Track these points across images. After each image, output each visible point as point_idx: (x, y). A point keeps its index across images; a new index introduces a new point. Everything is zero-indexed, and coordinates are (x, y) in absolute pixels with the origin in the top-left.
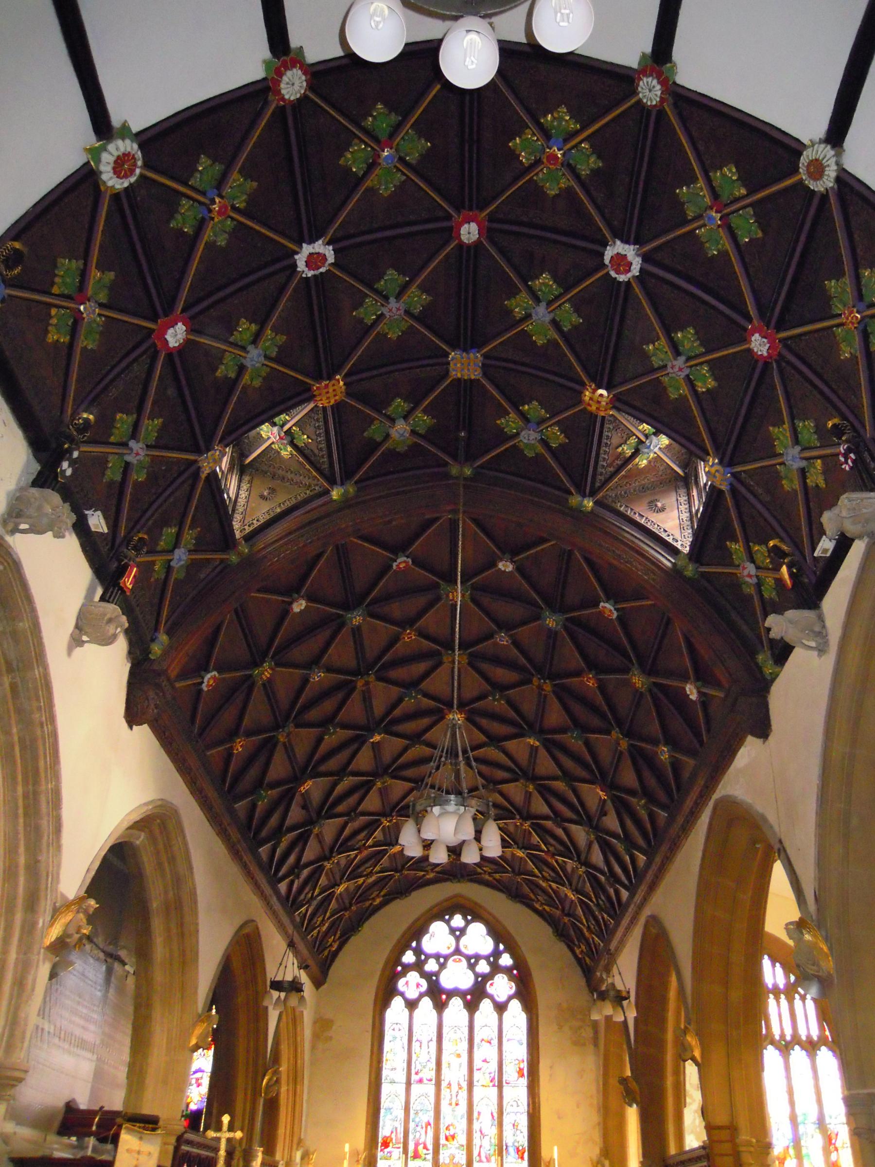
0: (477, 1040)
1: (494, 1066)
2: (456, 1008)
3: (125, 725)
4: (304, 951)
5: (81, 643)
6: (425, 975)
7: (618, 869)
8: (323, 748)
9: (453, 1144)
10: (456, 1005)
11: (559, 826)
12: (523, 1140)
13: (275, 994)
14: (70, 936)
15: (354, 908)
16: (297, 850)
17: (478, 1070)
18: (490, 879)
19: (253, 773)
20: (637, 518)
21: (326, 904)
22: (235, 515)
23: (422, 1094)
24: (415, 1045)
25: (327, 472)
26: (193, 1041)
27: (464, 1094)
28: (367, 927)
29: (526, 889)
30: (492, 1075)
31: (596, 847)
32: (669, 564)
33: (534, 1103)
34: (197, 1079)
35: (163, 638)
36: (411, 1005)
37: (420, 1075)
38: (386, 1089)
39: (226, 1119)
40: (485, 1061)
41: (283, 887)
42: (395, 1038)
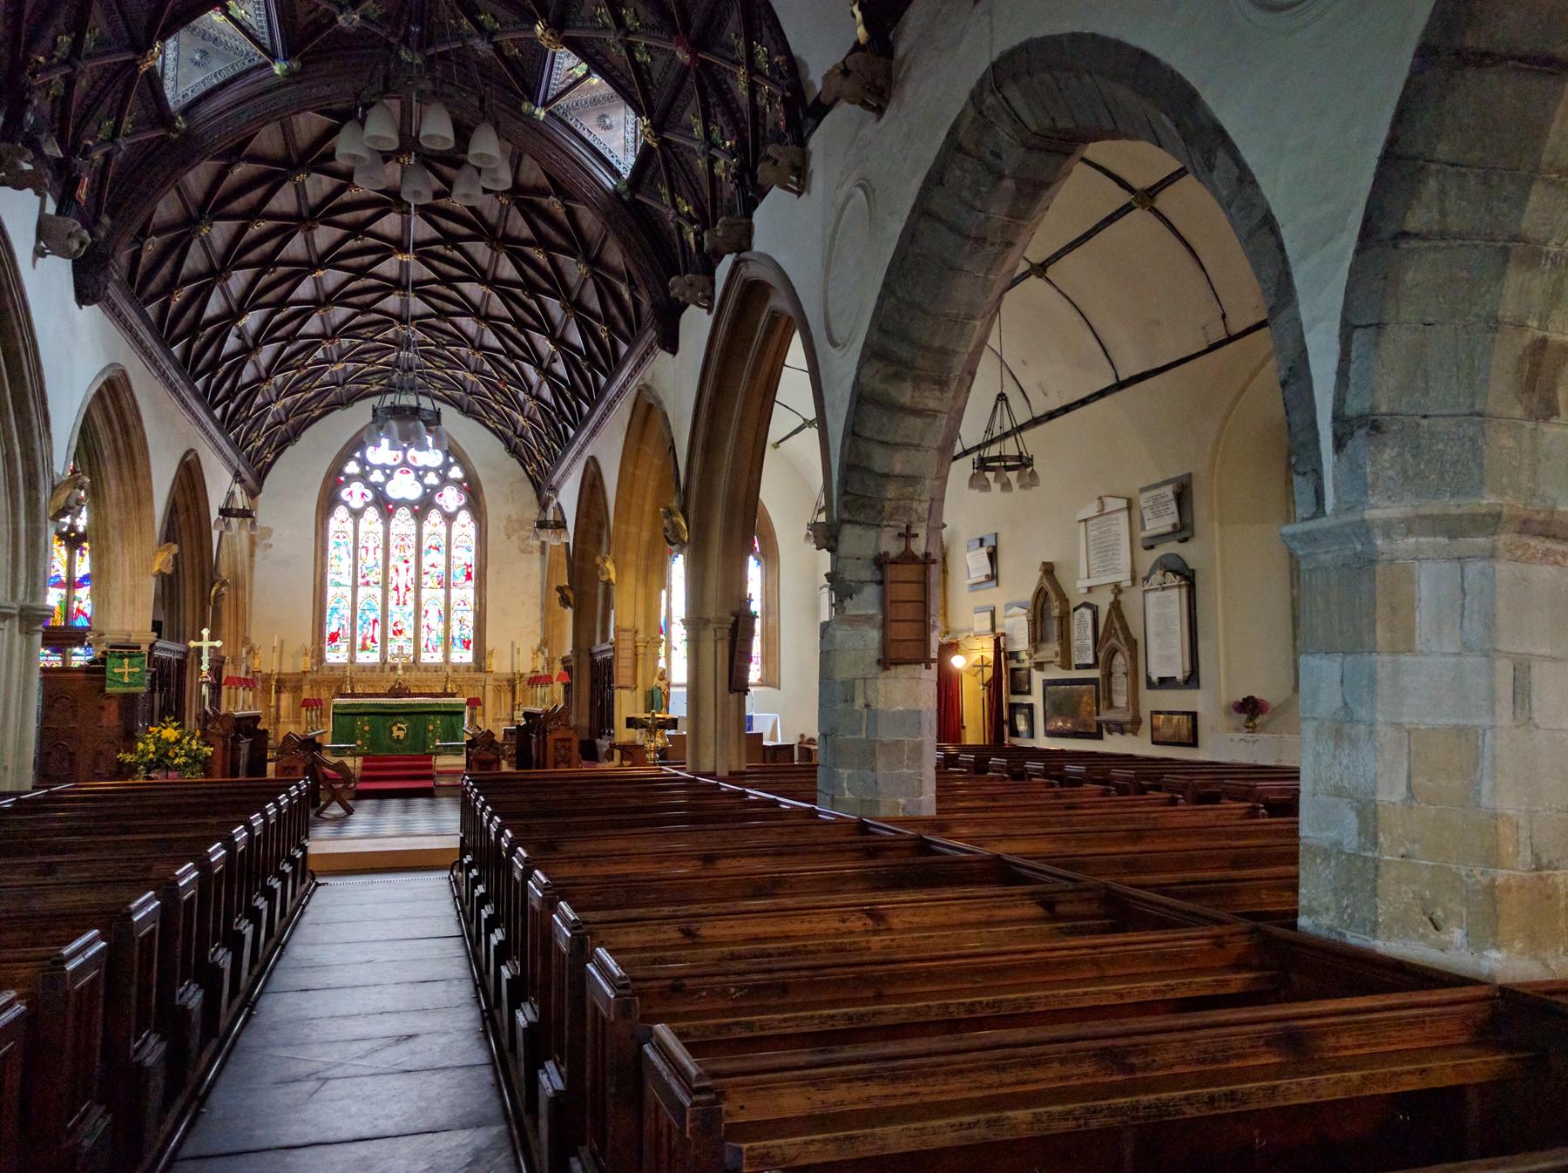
0: (425, 547)
1: (442, 569)
2: (403, 522)
3: (76, 306)
6: (370, 485)
7: (614, 310)
8: (246, 237)
9: (400, 640)
10: (403, 514)
11: (531, 296)
12: (469, 633)
15: (291, 421)
16: (174, 257)
19: (165, 270)
20: (585, 134)
23: (370, 595)
24: (362, 552)
25: (268, 47)
27: (411, 595)
28: (306, 436)
29: (477, 407)
31: (590, 285)
33: (480, 599)
35: (106, 220)
36: (356, 514)
37: (367, 578)
38: (331, 591)
39: (205, 632)
40: (433, 566)
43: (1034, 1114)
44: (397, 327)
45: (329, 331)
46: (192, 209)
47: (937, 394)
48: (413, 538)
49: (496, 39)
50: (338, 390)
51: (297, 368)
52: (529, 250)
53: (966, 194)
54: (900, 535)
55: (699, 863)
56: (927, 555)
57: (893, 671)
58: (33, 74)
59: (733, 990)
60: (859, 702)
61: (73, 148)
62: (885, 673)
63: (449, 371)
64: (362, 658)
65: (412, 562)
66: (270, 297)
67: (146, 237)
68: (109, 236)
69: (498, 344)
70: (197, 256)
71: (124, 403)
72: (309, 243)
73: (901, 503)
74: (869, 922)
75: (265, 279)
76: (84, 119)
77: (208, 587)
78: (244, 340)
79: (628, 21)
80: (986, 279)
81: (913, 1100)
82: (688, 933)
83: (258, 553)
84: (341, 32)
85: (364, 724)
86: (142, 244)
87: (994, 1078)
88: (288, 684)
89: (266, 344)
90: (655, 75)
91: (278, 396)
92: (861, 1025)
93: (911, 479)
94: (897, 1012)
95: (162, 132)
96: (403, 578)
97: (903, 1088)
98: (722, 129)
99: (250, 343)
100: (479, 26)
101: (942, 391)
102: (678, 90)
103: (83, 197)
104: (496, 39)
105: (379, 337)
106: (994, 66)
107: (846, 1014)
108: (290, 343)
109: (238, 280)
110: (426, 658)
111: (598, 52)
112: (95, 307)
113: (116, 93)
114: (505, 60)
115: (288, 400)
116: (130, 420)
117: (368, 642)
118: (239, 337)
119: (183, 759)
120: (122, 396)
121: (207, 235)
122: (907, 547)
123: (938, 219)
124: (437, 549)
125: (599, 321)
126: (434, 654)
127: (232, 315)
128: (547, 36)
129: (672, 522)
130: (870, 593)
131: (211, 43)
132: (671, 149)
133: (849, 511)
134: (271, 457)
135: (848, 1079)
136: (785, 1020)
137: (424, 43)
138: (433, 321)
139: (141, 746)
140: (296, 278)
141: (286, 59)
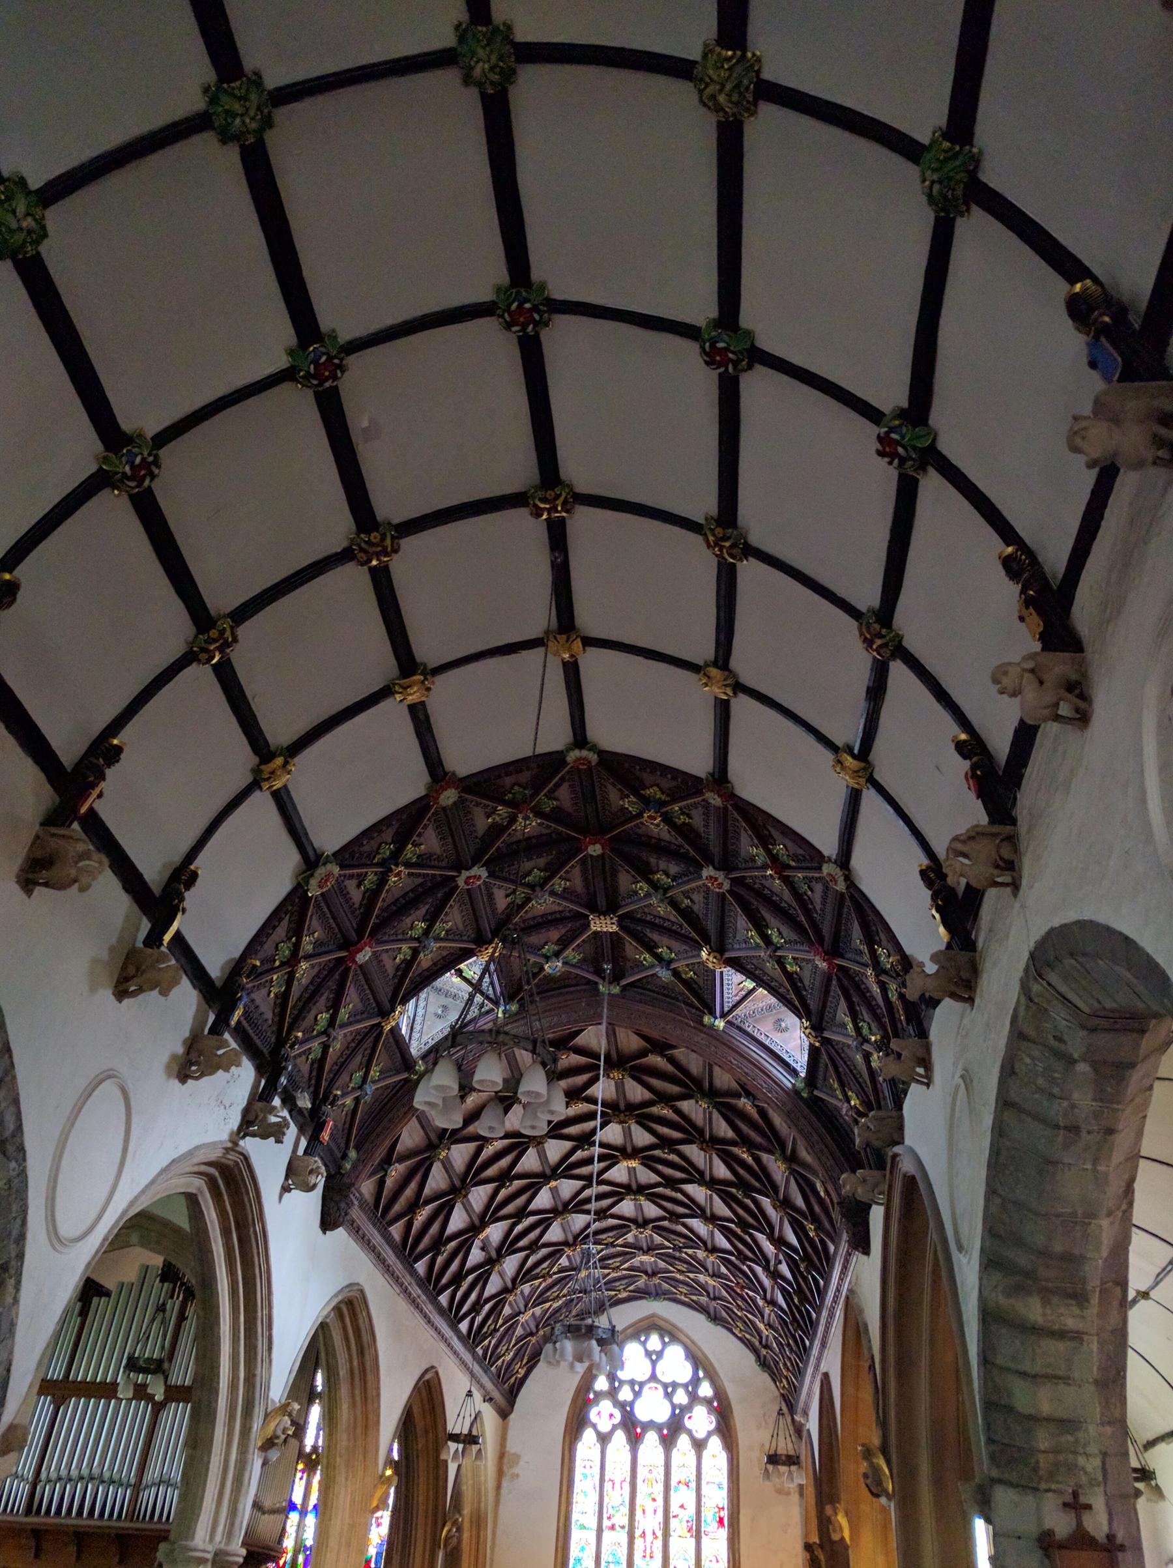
0: (673, 1483)
3: (320, 1232)
4: (489, 1385)
5: (289, 1190)
13: (453, 1446)
14: (277, 1437)
15: (541, 1333)
16: (418, 1178)
17: (674, 1517)
18: (686, 1300)
19: (409, 1191)
20: (762, 1038)
21: (510, 1332)
22: (412, 1042)
24: (608, 1486)
25: (492, 996)
26: (375, 1504)
27: (659, 1544)
30: (689, 1524)
32: (790, 1085)
34: (377, 1518)
35: (353, 1154)
36: (604, 1439)
37: (613, 1521)
40: (682, 1506)
41: (464, 1326)
42: (586, 1477)
44: (634, 1232)
45: (571, 1239)
46: (433, 1137)
47: (1077, 1311)
48: (662, 1470)
49: (673, 966)
51: (543, 1277)
52: (735, 1150)
53: (1040, 1081)
54: (1065, 1505)
56: (1110, 1537)
58: (292, 1047)
61: (321, 1099)
63: (691, 1275)
66: (510, 1208)
68: (354, 1167)
69: (727, 1246)
70: (438, 1178)
71: (361, 1321)
72: (542, 1156)
73: (1061, 1458)
75: (503, 1193)
76: (337, 1074)
77: (439, 1527)
78: (488, 1253)
79: (775, 939)
80: (1095, 1171)
83: (505, 1484)
84: (549, 979)
86: (386, 1171)
89: (509, 1255)
90: (807, 982)
91: (526, 1306)
93: (1067, 1425)
95: (405, 1075)
96: (649, 1522)
98: (868, 1024)
99: (494, 1254)
100: (659, 958)
101: (1081, 1306)
102: (827, 991)
103: (327, 1138)
104: (673, 966)
105: (620, 1241)
106: (1032, 956)
108: (533, 1252)
109: (478, 1196)
111: (756, 968)
113: (366, 1050)
114: (685, 982)
115: (538, 1310)
116: (366, 1338)
118: (483, 1249)
120: (360, 1316)
121: (447, 1157)
122: (1079, 1524)
124: (687, 1485)
125: (806, 1219)
127: (474, 1229)
128: (711, 959)
131: (451, 1000)
133: (998, 1467)
134: (522, 1372)
137: (616, 978)
138: (665, 1223)
140: (533, 1189)
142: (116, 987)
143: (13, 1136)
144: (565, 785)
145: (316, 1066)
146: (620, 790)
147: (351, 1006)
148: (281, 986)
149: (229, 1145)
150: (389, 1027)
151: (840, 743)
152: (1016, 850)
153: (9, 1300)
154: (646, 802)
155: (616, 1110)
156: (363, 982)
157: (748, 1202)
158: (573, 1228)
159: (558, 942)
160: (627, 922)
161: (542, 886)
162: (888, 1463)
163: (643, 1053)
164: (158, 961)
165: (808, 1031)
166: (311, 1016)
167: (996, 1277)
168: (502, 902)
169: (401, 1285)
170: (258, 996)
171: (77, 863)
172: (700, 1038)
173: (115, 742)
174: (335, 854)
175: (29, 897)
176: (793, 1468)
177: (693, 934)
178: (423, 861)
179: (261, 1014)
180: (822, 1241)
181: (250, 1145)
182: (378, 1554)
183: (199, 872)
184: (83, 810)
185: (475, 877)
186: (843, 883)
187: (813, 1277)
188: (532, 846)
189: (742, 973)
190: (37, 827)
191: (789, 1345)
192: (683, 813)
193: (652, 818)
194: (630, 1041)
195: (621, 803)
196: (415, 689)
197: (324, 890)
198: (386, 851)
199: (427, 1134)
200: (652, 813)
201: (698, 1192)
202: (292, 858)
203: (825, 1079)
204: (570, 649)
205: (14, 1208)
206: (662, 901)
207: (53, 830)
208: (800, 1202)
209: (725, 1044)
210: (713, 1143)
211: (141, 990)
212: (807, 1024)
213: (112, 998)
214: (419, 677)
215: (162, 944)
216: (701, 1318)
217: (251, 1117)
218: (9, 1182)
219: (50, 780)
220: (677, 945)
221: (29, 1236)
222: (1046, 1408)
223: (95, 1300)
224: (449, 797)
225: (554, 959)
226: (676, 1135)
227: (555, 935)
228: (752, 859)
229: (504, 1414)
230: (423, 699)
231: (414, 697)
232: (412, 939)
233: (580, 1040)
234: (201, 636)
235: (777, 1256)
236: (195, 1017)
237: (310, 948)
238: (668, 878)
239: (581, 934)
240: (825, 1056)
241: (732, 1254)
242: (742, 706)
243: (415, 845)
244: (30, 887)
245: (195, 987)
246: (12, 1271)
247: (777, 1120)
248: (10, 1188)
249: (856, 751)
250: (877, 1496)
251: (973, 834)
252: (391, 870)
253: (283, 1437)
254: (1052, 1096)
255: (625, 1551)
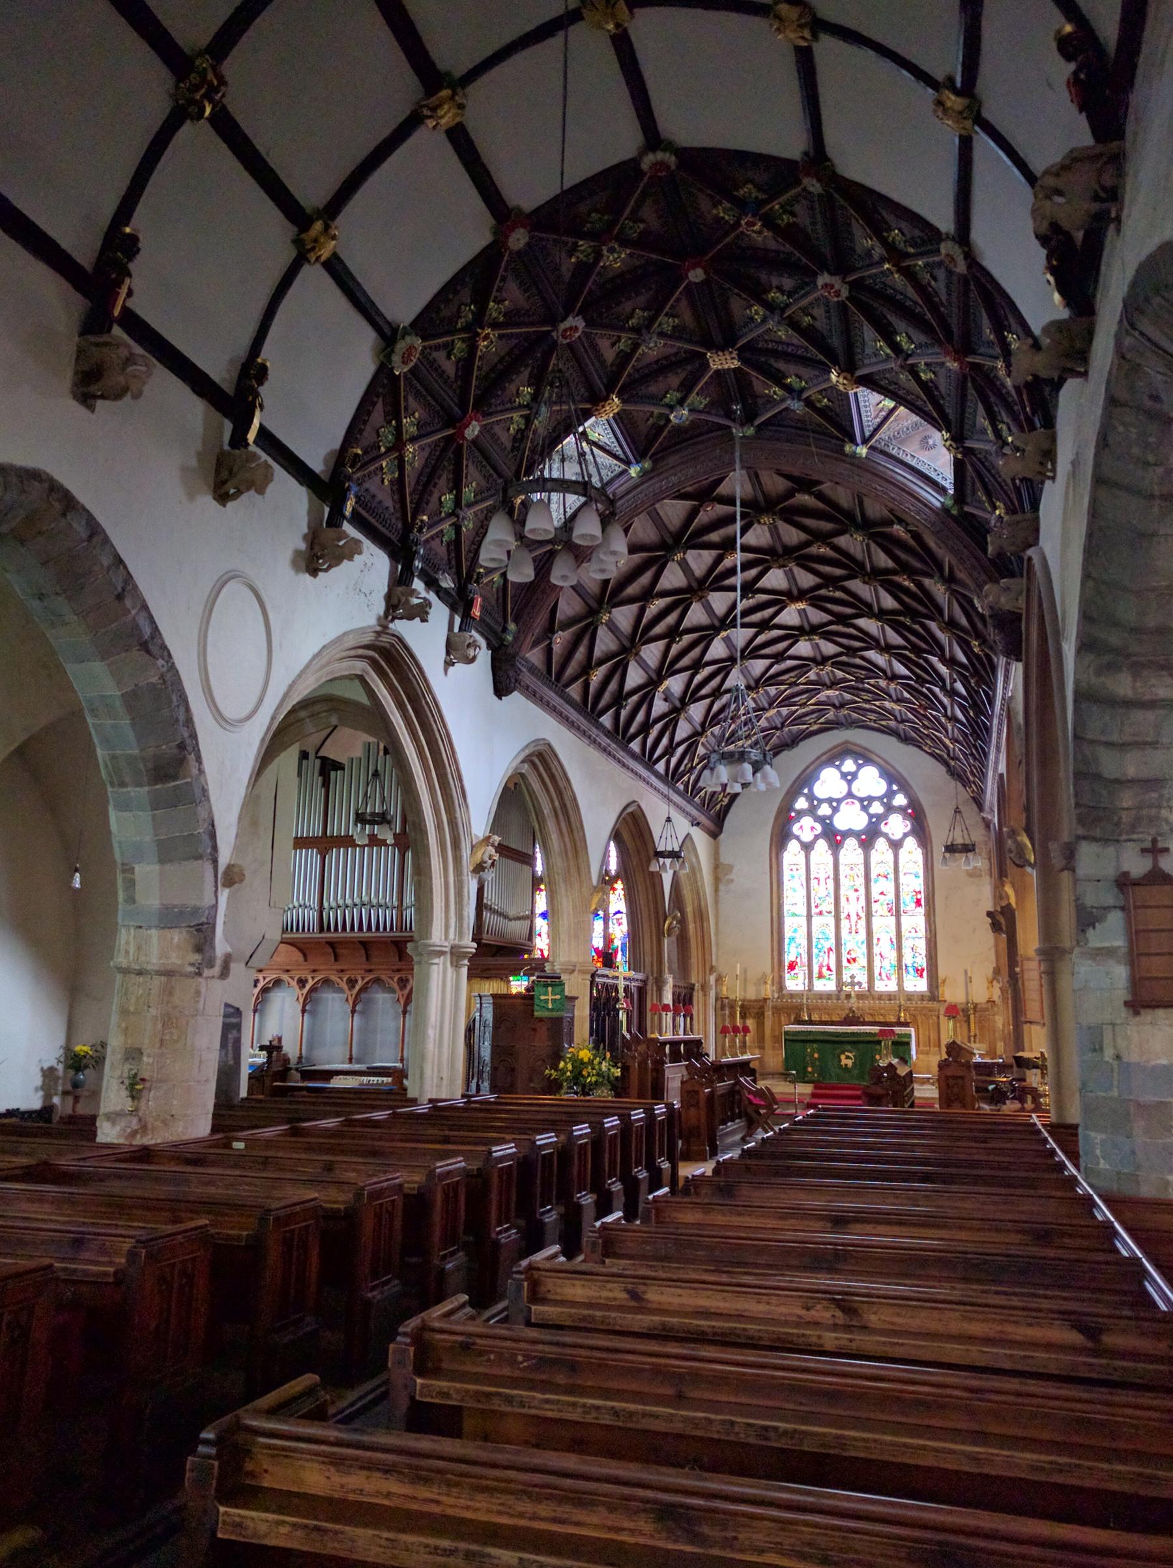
0: (873, 875)
1: (891, 896)
2: (851, 851)
4: (695, 812)
5: (453, 664)
6: (819, 819)
10: (851, 844)
12: (922, 962)
16: (585, 642)
20: (908, 460)
23: (823, 925)
24: (813, 883)
25: (622, 456)
27: (863, 922)
32: (938, 504)
35: (512, 627)
36: (807, 847)
40: (882, 893)
43: (521, 1559)
48: (862, 868)
49: (805, 395)
50: (778, 733)
52: (897, 579)
53: (1135, 450)
54: (1144, 851)
55: (829, 1225)
57: (1147, 1016)
58: (420, 530)
59: (520, 1358)
60: (1109, 1054)
62: (1138, 1019)
63: (877, 703)
64: (820, 986)
65: (862, 890)
66: (685, 661)
67: (553, 633)
68: (516, 638)
69: (906, 672)
71: (554, 770)
73: (1145, 812)
74: (839, 1314)
79: (905, 346)
81: (436, 1509)
82: (634, 1295)
83: (722, 887)
84: (678, 429)
85: (813, 1052)
87: (527, 1506)
88: (752, 1010)
92: (630, 1425)
94: (670, 1419)
96: (853, 906)
97: (424, 1492)
98: (1008, 425)
100: (789, 389)
102: (963, 397)
103: (478, 614)
104: (805, 395)
105: (802, 680)
107: (613, 1408)
109: (652, 653)
110: (880, 986)
111: (891, 383)
112: (516, 694)
116: (562, 783)
117: (824, 970)
118: (666, 700)
119: (594, 1079)
123: (1116, 485)
124: (886, 877)
125: (971, 636)
126: (887, 982)
128: (841, 380)
129: (1016, 841)
130: (1115, 919)
132: (975, 455)
133: (1083, 825)
135: (370, 1467)
136: (547, 1401)
137: (749, 417)
138: (844, 658)
139: (562, 1064)
141: (638, 462)
142: (215, 492)
143: (152, 638)
144: (649, 201)
145: (452, 547)
146: (712, 197)
147: (474, 484)
148: (393, 472)
149: (379, 629)
150: (519, 501)
151: (939, 75)
152: (1120, 173)
153: (195, 771)
154: (741, 205)
155: (765, 558)
156: (480, 458)
157: (917, 627)
158: (753, 673)
159: (682, 384)
160: (747, 355)
161: (648, 327)
162: (1031, 839)
163: (790, 494)
164: (247, 461)
165: (948, 443)
166: (434, 499)
167: (1090, 657)
168: (609, 355)
169: (589, 737)
170: (372, 485)
171: (124, 369)
172: (842, 468)
173: (128, 230)
174: (413, 324)
175: (93, 411)
176: (970, 855)
177: (821, 357)
178: (512, 318)
179: (380, 502)
180: (987, 656)
181: (400, 626)
182: (623, 945)
183: (268, 364)
184: (116, 312)
185: (571, 328)
186: (963, 262)
187: (984, 691)
188: (624, 284)
189: (879, 392)
190: (77, 338)
191: (972, 754)
192: (786, 211)
193: (750, 224)
194: (775, 484)
195: (715, 212)
196: (446, 107)
197: (412, 364)
198: (468, 313)
199: (585, 602)
200: (749, 218)
201: (870, 625)
202: (367, 337)
203: (974, 492)
204: (613, 16)
205: (174, 698)
206: (779, 323)
207: (92, 338)
208: (964, 621)
209: (868, 471)
210: (876, 575)
211: (239, 493)
212: (947, 435)
213: (214, 503)
214: (445, 93)
215: (248, 444)
216: (893, 740)
217: (394, 601)
218: (162, 676)
219: (77, 287)
220: (806, 372)
221: (196, 719)
222: (1131, 771)
223: (333, 774)
224: (518, 239)
225: (678, 407)
226: (838, 572)
227: (675, 380)
228: (869, 253)
229: (715, 834)
230: (458, 119)
231: (447, 117)
232: (521, 406)
233: (723, 489)
234: (182, 85)
235: (951, 675)
236: (309, 513)
237: (413, 430)
238: (783, 294)
239: (702, 375)
240: (969, 467)
241: (910, 678)
242: (827, 49)
243: (499, 301)
244: (89, 401)
245: (301, 484)
246: (190, 748)
247: (931, 543)
248: (164, 682)
249: (959, 85)
250: (1022, 866)
251: (1067, 162)
252: (478, 335)
253: (490, 862)
254: (1147, 464)
255: (833, 930)
